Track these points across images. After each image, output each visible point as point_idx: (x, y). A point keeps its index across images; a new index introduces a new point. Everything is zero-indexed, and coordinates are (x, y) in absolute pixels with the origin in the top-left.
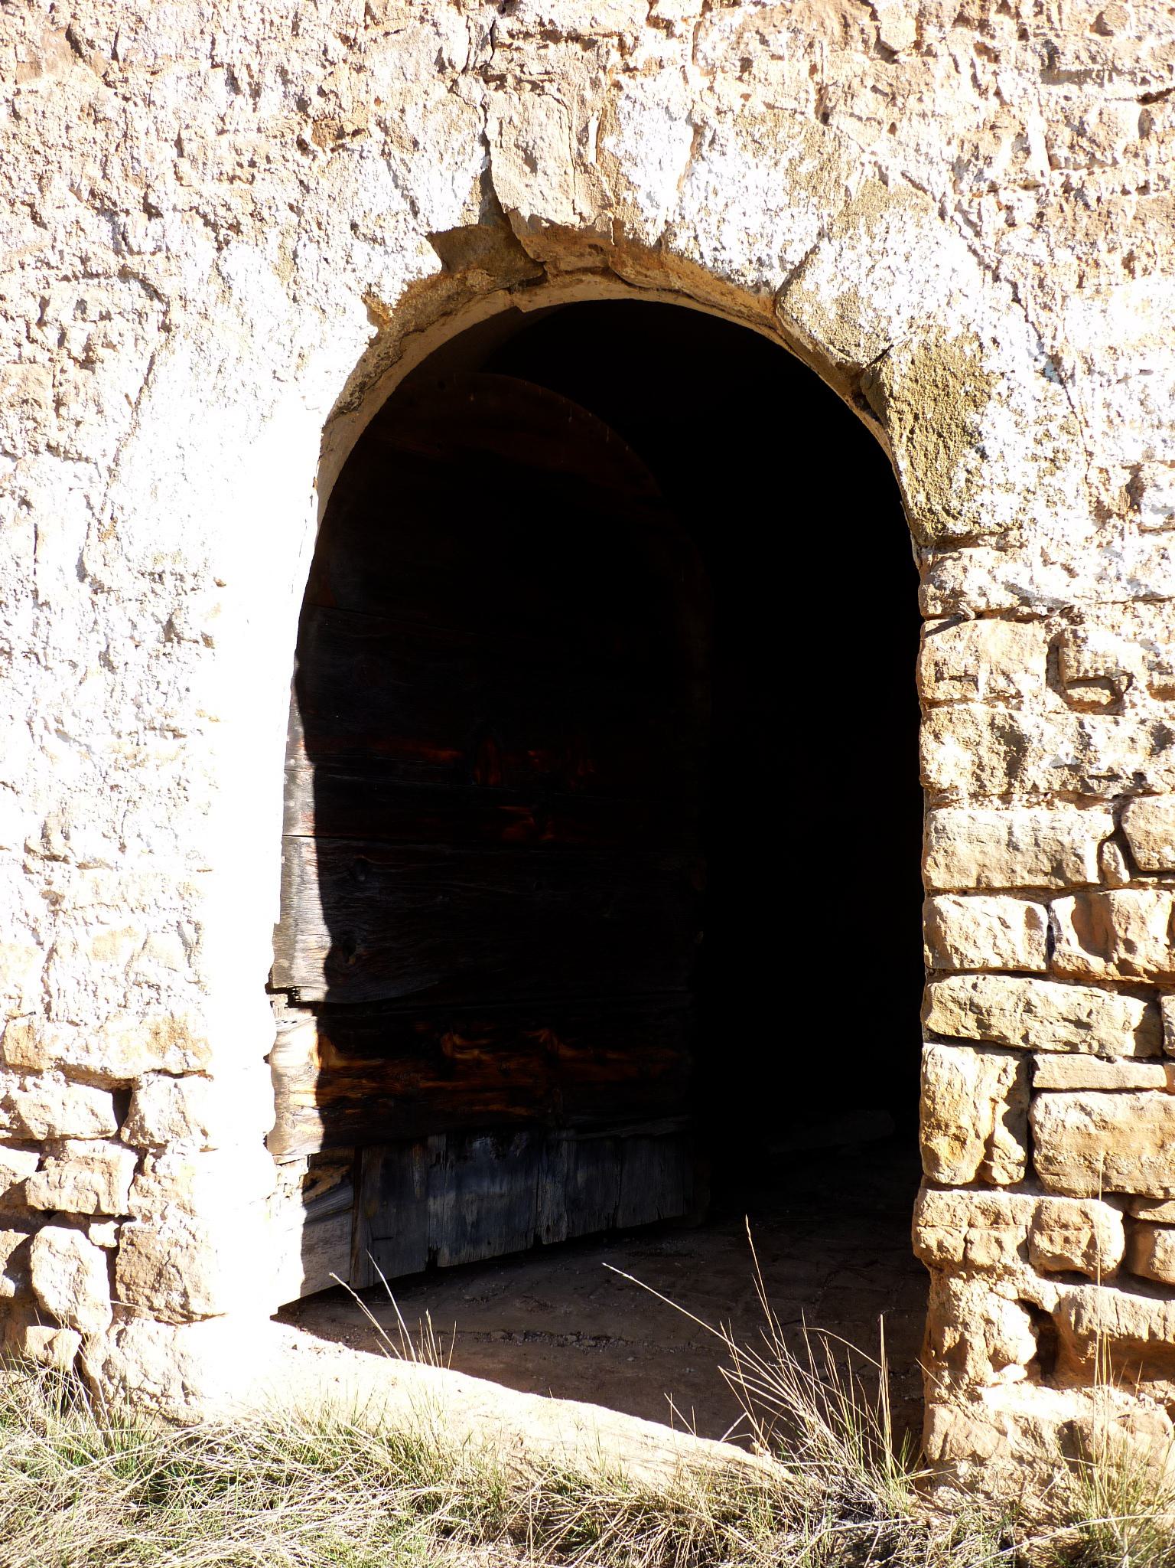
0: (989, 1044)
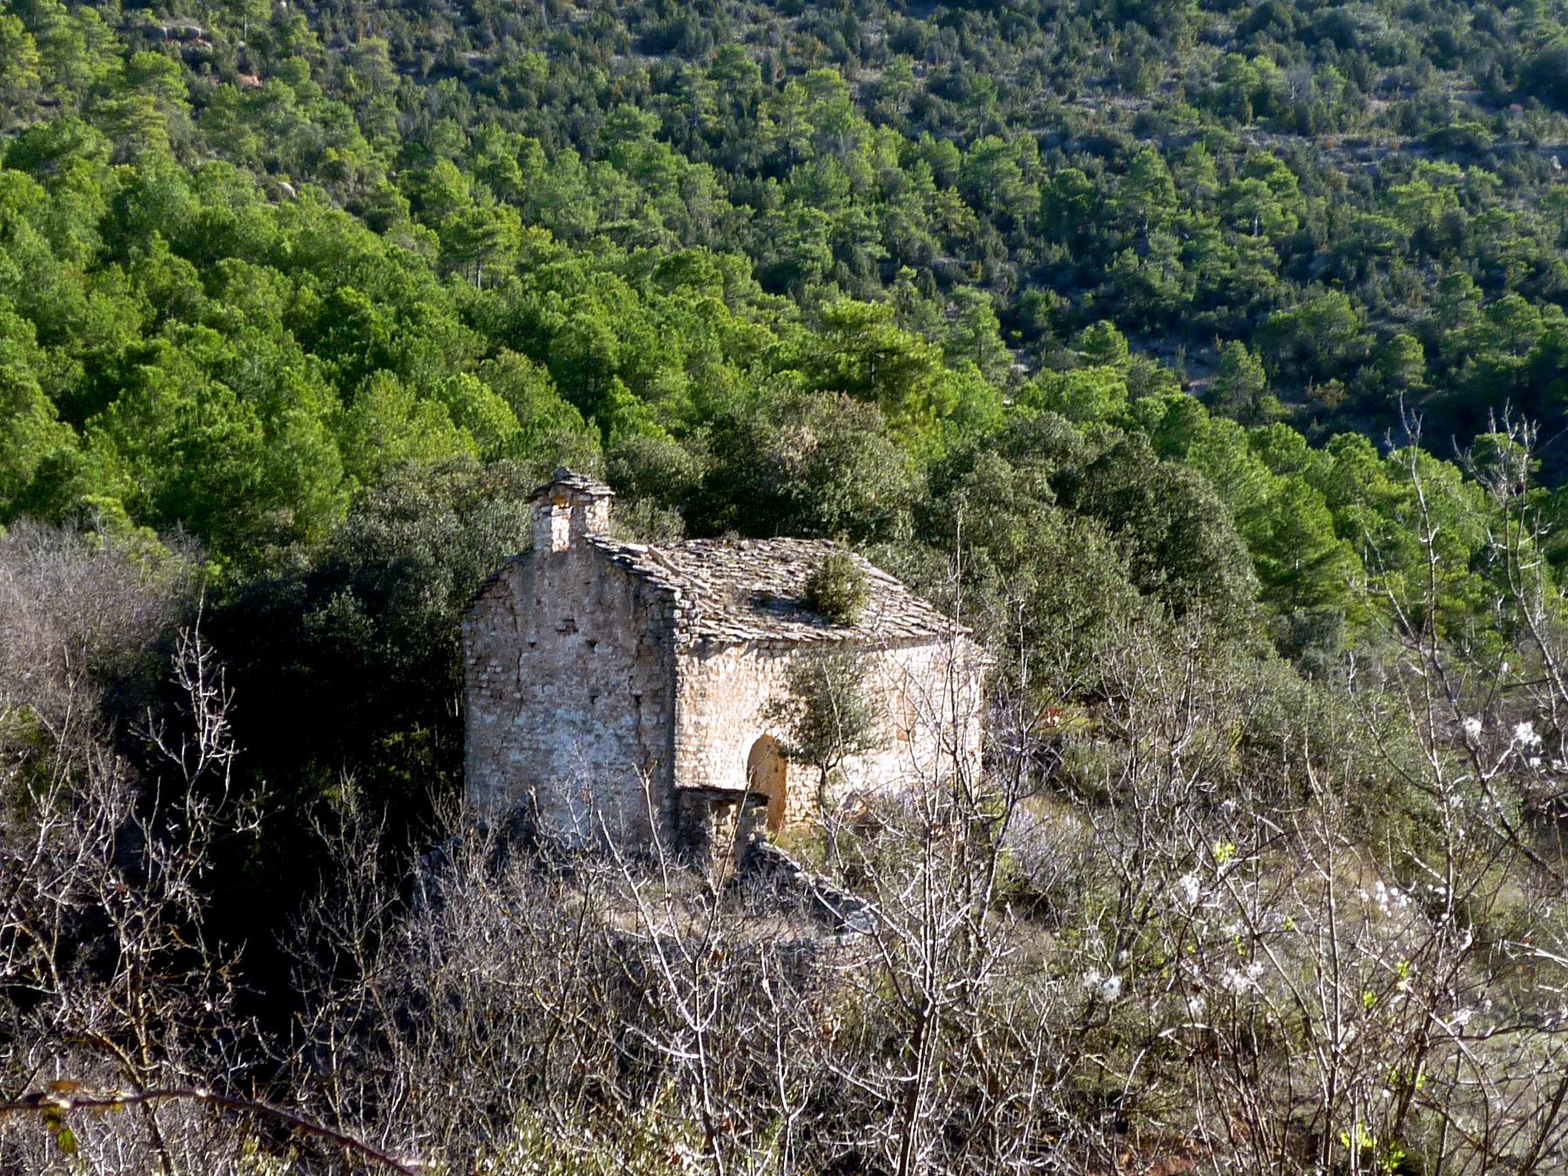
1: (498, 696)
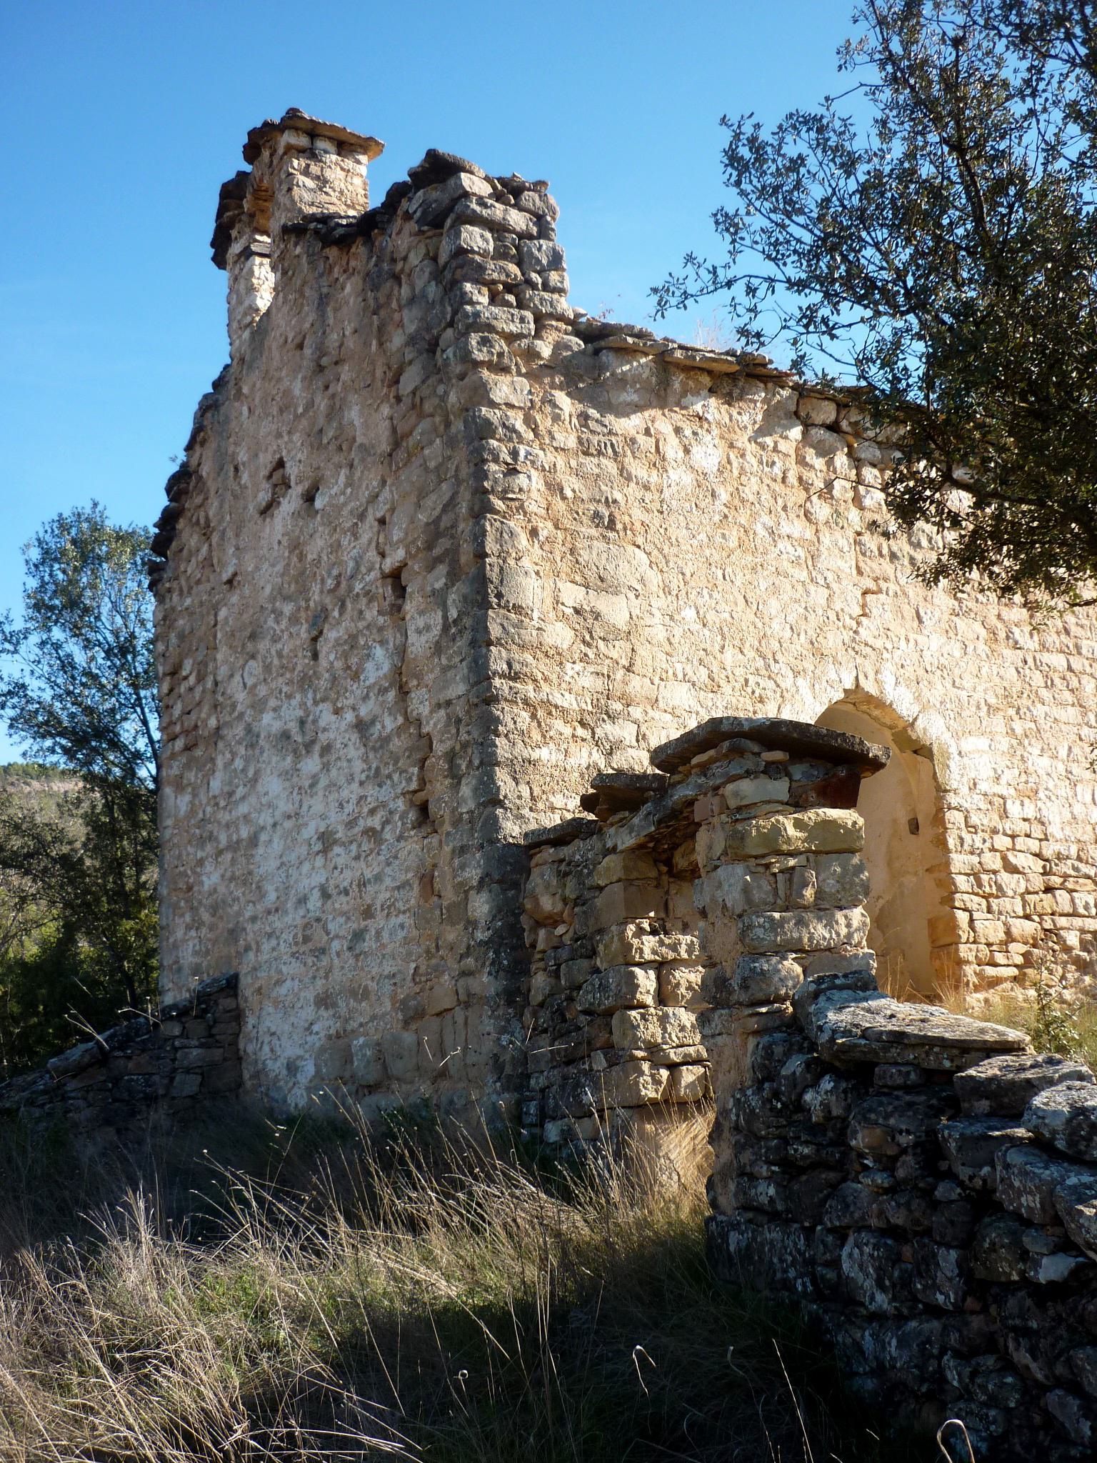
0: (965, 910)
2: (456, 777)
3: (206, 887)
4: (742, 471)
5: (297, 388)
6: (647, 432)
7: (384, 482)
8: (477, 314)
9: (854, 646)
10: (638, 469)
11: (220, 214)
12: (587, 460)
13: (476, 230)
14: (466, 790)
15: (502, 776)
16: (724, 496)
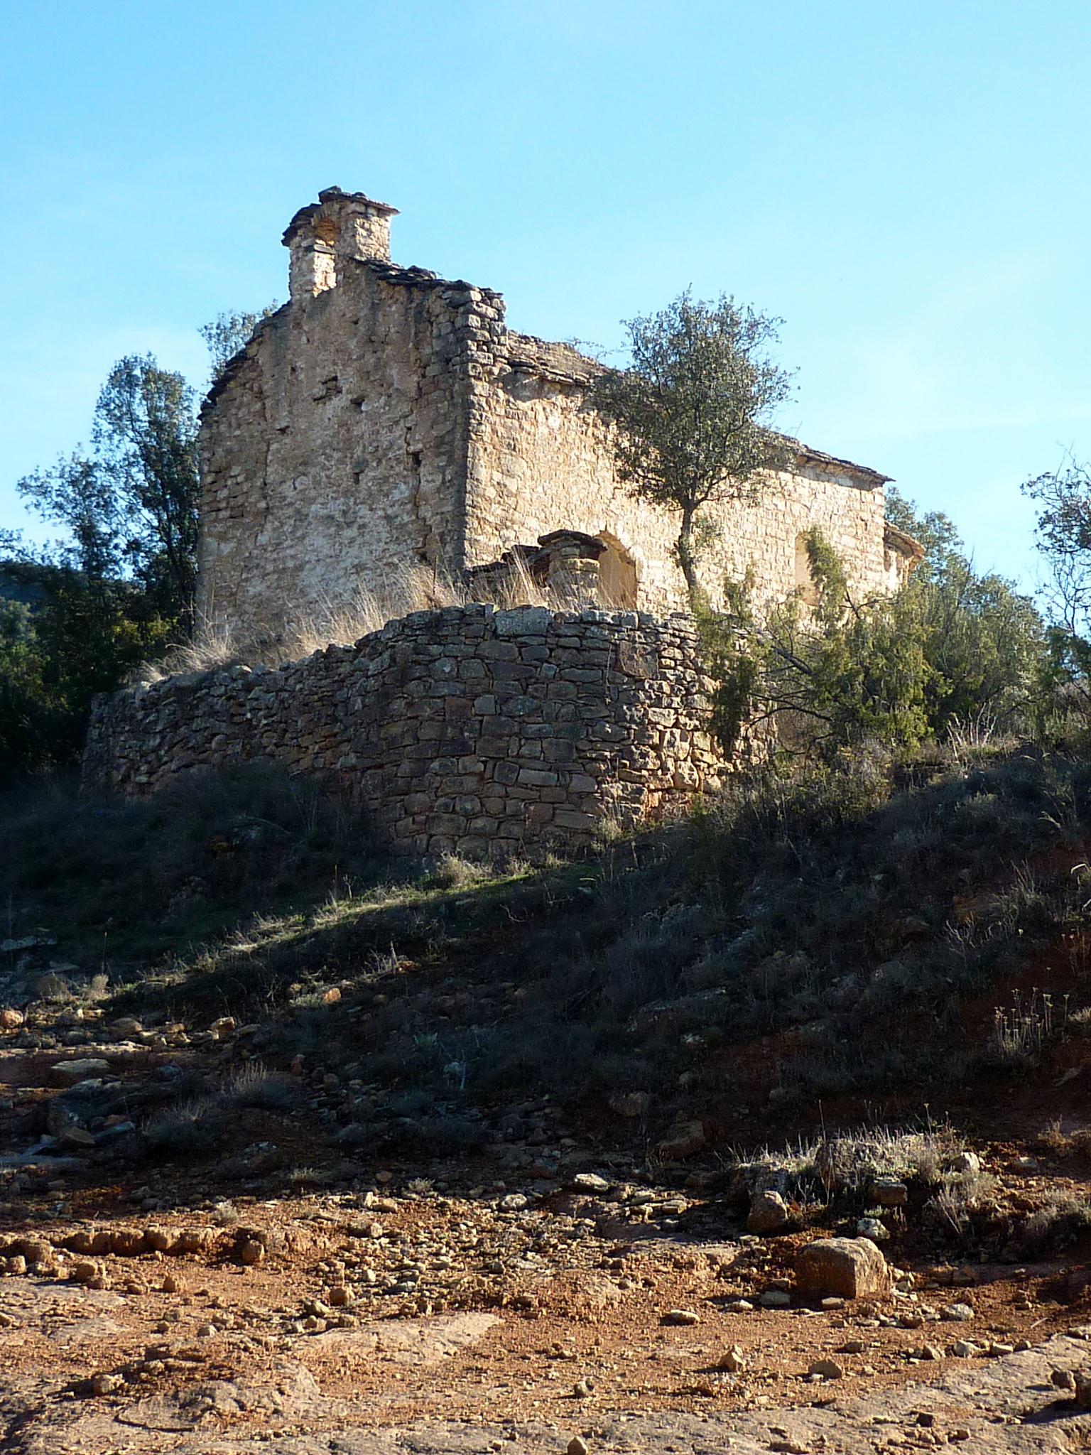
1: (238, 515)
2: (444, 543)
3: (251, 593)
4: (569, 429)
5: (352, 344)
6: (532, 410)
7: (412, 411)
8: (472, 355)
9: (606, 512)
10: (527, 426)
11: (294, 220)
12: (506, 420)
13: (474, 317)
14: (448, 548)
15: (466, 544)
16: (560, 439)
